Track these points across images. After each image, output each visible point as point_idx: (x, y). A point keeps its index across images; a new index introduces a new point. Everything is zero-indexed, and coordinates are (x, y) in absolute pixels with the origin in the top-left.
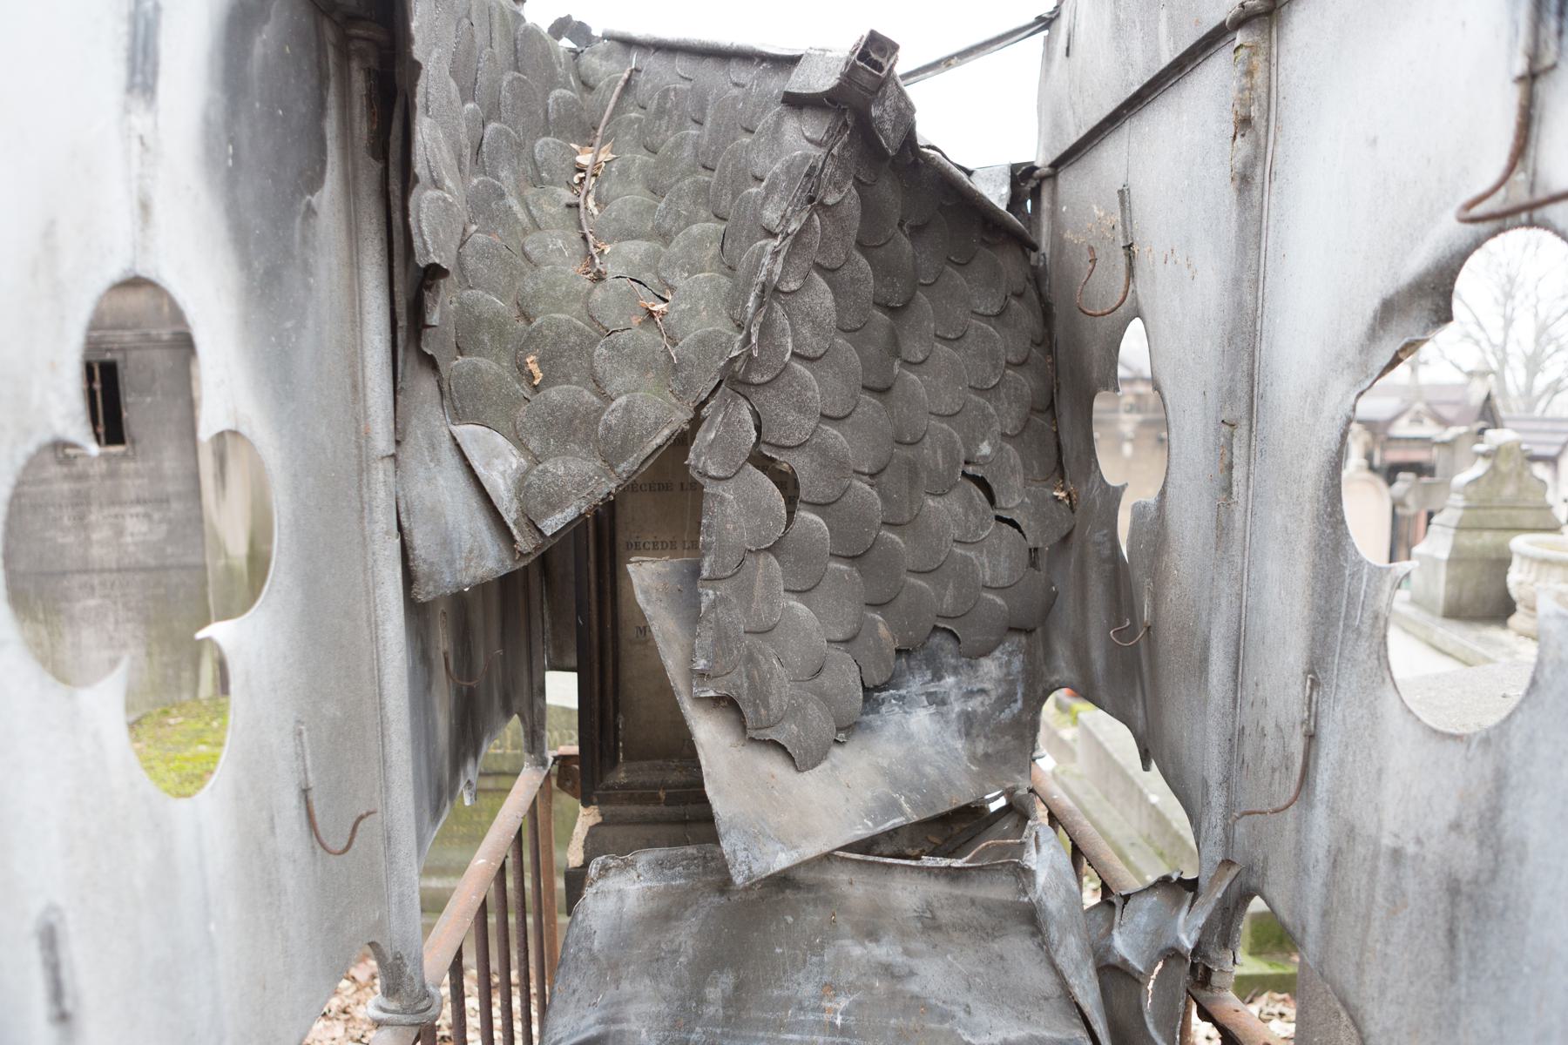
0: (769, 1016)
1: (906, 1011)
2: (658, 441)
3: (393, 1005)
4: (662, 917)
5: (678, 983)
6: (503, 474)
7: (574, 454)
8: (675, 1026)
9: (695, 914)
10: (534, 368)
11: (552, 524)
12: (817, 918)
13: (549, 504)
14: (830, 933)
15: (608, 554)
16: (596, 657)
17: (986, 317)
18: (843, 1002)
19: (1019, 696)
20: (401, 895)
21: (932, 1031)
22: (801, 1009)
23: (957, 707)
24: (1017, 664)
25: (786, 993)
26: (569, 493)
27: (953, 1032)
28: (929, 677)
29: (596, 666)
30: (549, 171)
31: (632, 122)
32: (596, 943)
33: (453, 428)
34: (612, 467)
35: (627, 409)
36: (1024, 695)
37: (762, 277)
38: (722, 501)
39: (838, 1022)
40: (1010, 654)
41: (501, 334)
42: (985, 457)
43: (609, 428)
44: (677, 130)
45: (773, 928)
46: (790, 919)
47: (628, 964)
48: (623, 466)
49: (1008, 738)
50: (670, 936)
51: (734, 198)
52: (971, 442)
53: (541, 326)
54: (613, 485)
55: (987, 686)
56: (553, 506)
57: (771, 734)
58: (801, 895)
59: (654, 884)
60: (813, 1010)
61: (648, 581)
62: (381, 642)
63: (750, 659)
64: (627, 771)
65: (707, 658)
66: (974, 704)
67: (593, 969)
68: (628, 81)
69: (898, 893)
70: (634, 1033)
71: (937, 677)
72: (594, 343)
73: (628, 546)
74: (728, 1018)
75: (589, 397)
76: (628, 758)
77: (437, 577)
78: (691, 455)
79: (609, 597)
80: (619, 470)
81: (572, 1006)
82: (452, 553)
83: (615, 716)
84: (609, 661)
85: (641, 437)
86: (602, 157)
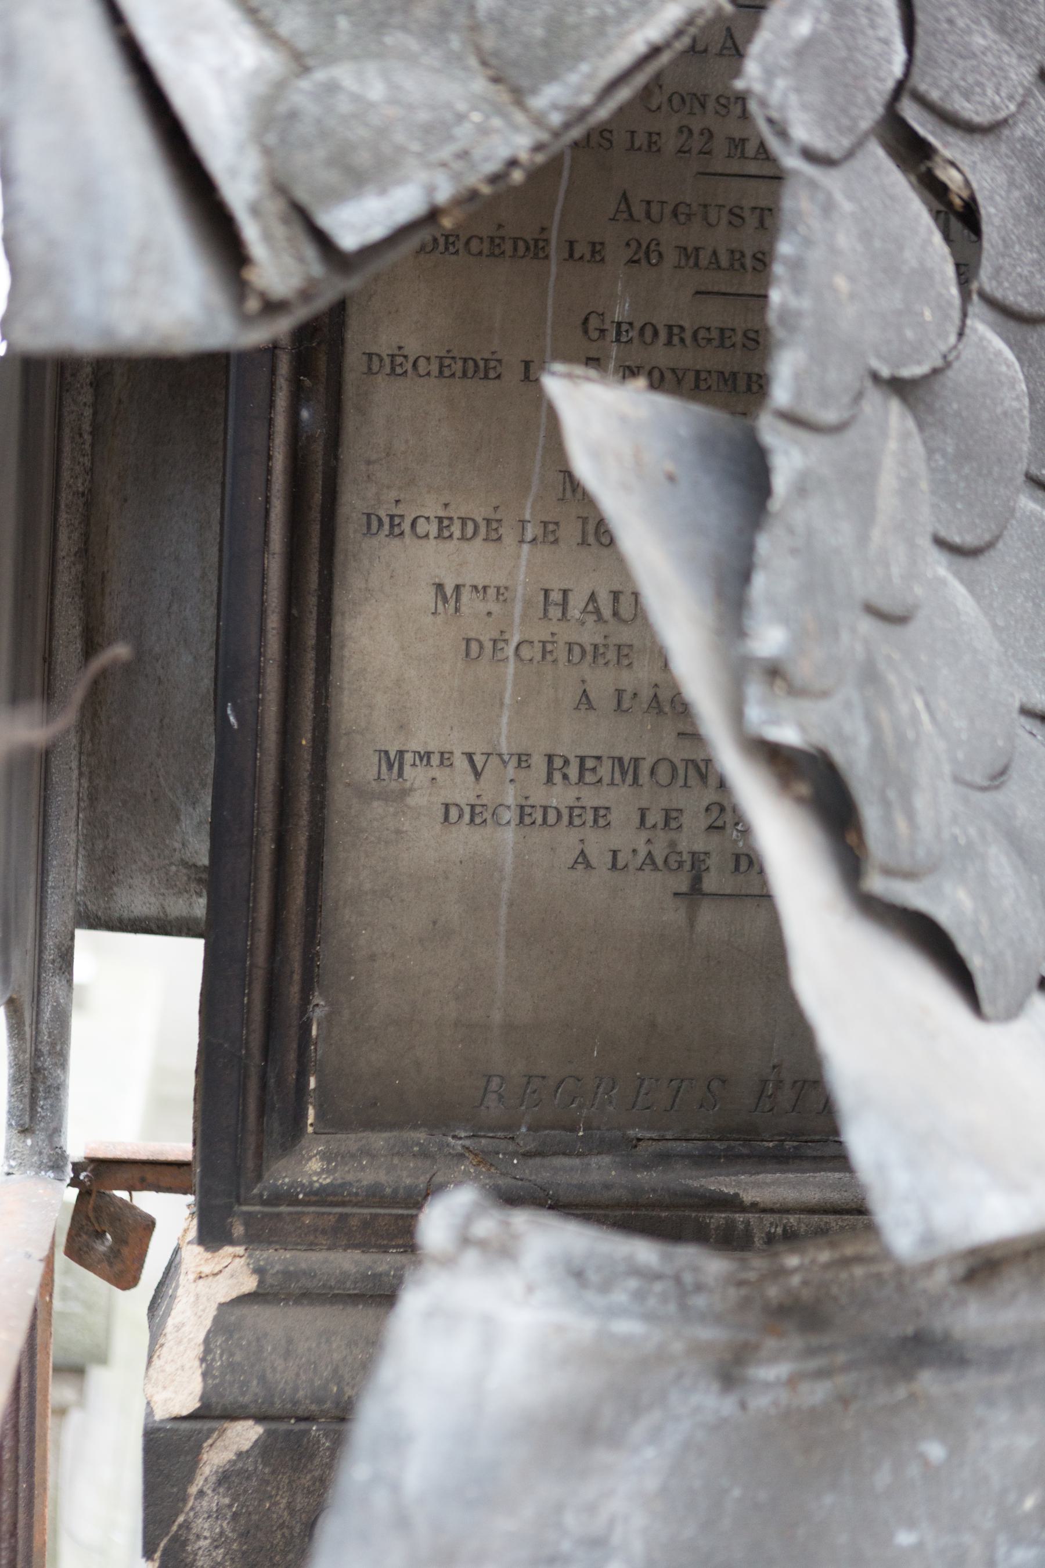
4: (580, 1430)
6: (220, 74)
7: (411, 59)
9: (655, 1435)
15: (315, 540)
26: (401, 150)
29: (268, 846)
34: (519, 96)
38: (828, 208)
45: (883, 1478)
46: (935, 1451)
56: (359, 177)
57: (913, 896)
58: (970, 1382)
63: (870, 676)
64: (326, 1157)
65: (785, 620)
73: (371, 523)
76: (330, 1122)
79: (310, 658)
85: (602, 21)
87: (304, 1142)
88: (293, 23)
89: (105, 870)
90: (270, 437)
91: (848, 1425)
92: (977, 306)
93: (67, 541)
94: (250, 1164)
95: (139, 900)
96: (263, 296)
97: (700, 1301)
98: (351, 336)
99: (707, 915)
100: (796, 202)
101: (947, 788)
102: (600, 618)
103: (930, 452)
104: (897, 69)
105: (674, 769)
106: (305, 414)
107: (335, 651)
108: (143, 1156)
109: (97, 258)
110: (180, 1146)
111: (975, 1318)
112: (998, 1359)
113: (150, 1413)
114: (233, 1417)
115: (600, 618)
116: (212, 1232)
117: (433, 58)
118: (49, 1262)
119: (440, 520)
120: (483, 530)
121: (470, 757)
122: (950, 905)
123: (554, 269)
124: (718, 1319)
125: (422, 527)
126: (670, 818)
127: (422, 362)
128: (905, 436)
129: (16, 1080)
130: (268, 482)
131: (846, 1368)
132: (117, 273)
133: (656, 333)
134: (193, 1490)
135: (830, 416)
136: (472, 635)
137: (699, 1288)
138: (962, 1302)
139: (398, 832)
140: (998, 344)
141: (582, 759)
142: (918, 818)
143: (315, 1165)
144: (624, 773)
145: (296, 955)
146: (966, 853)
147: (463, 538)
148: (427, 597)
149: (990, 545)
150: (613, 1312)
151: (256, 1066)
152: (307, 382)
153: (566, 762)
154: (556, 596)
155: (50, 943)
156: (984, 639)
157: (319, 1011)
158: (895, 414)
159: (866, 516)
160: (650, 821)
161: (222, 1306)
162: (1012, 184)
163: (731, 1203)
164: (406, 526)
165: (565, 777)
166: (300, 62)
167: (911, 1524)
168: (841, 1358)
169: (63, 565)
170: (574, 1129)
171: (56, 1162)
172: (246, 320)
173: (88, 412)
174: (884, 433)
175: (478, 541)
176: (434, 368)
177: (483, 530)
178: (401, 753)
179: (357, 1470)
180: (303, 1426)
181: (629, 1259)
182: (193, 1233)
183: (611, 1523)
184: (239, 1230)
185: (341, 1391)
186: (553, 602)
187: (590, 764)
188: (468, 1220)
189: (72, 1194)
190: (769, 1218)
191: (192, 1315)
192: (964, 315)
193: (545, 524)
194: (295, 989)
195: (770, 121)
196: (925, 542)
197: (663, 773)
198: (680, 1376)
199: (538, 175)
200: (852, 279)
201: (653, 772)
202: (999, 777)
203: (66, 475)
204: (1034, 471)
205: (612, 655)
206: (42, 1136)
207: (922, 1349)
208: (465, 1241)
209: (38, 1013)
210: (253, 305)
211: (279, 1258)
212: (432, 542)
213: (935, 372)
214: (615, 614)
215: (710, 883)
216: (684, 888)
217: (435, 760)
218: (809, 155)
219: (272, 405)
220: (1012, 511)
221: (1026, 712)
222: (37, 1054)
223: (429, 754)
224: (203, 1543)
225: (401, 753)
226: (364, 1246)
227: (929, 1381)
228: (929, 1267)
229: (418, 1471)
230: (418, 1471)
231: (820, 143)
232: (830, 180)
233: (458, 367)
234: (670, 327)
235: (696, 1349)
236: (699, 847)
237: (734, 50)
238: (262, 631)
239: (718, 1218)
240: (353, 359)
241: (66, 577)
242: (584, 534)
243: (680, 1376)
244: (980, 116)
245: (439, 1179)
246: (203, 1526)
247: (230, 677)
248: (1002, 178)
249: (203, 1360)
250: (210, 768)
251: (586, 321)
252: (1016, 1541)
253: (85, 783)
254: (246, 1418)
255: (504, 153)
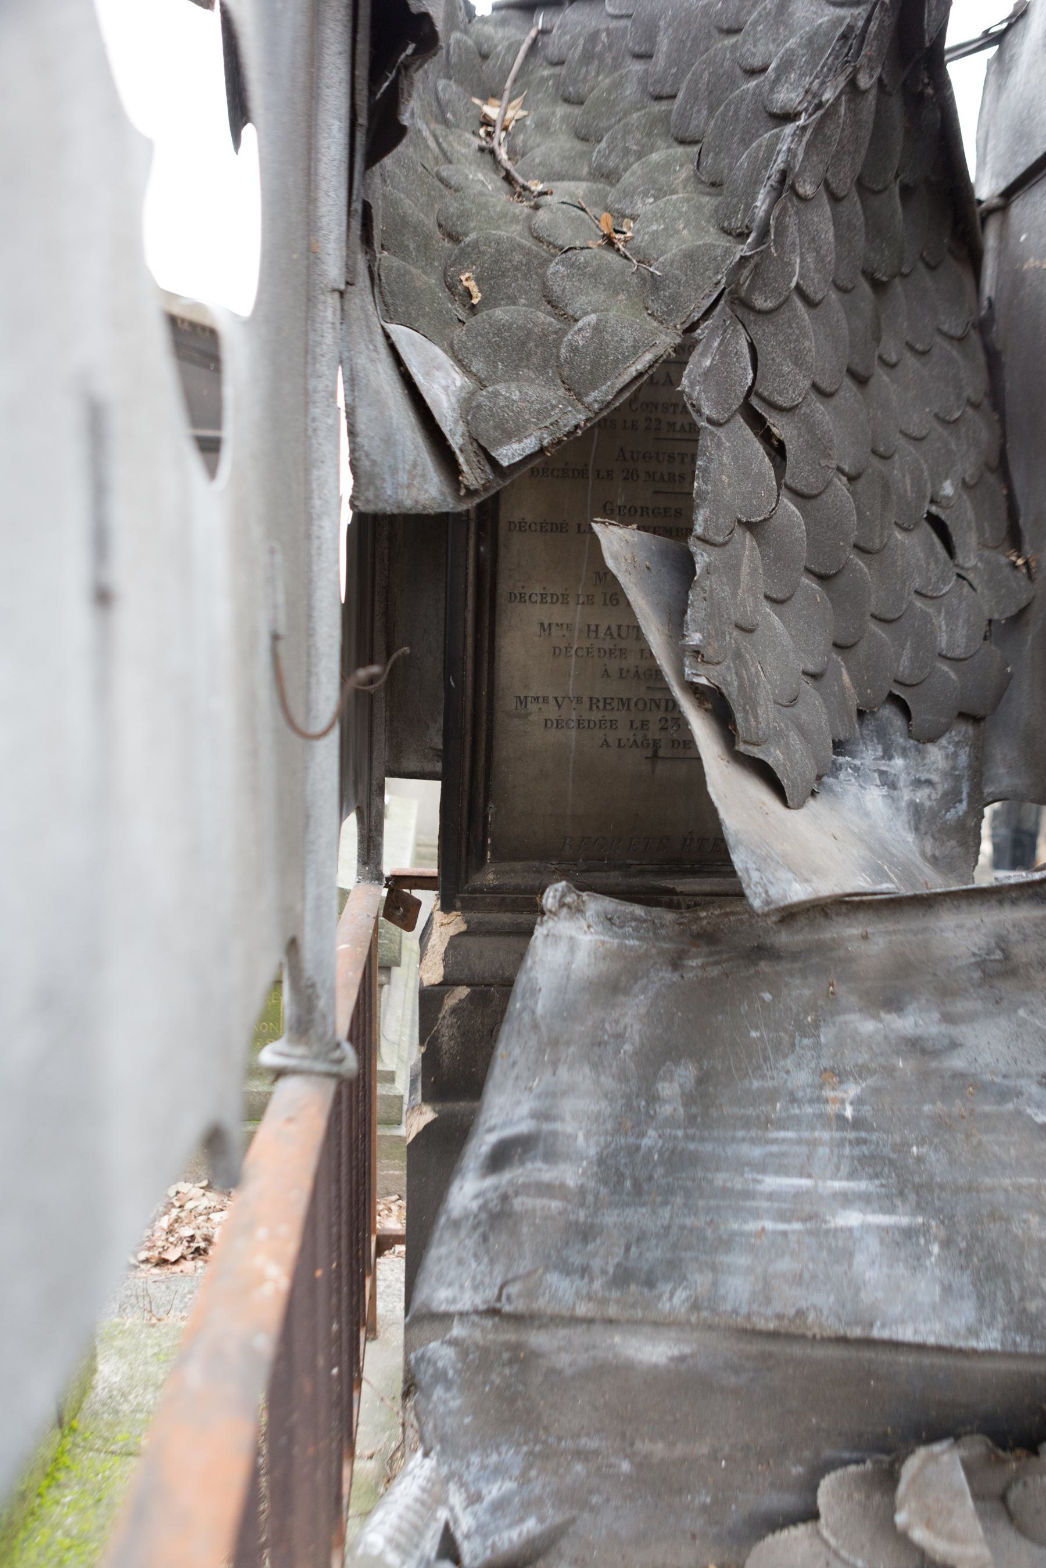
0: (750, 1111)
1: (945, 1094)
2: (640, 366)
3: (300, 1050)
4: (609, 988)
5: (622, 1077)
6: (446, 388)
7: (532, 381)
8: (619, 1129)
9: (644, 990)
10: (472, 285)
11: (508, 454)
12: (807, 992)
13: (504, 431)
14: (827, 1007)
16: (468, 727)
17: (951, 338)
18: (853, 1090)
19: (964, 795)
20: (319, 898)
21: (986, 1116)
22: (793, 1099)
23: (906, 795)
24: (963, 759)
25: (770, 1084)
26: (528, 421)
27: (1019, 1113)
28: (880, 753)
29: (468, 739)
30: (454, 114)
31: (544, 80)
32: (540, 1004)
33: (386, 325)
34: (579, 397)
35: (598, 329)
36: (969, 796)
37: (779, 163)
38: (719, 444)
39: (849, 1112)
40: (957, 744)
41: (426, 247)
42: (947, 498)
43: (574, 349)
44: (611, 73)
45: (744, 1008)
46: (767, 996)
47: (568, 1044)
48: (594, 394)
49: (953, 843)
50: (615, 1014)
51: (712, 110)
52: (937, 480)
53: (477, 241)
54: (581, 417)
55: (935, 777)
56: (509, 435)
58: (782, 966)
59: (606, 939)
60: (811, 1101)
61: (616, 547)
62: (316, 543)
63: (738, 655)
64: (495, 873)
65: (701, 630)
66: (921, 795)
67: (533, 1042)
68: (535, 41)
69: (949, 935)
70: (569, 1136)
71: (888, 755)
72: (545, 263)
74: (691, 1120)
75: (543, 317)
76: (498, 858)
77: (378, 482)
78: (685, 381)
80: (588, 399)
81: (510, 1083)
82: (395, 458)
83: (486, 805)
84: (483, 736)
85: (616, 361)
86: (510, 114)
87: (486, 867)
88: (478, 366)
89: (397, 751)
90: (467, 559)
91: (728, 985)
92: (784, 491)
93: (378, 609)
94: (463, 876)
95: (412, 766)
96: (467, 488)
97: (663, 932)
98: (503, 513)
99: (660, 766)
100: (706, 442)
101: (771, 705)
102: (612, 637)
103: (763, 557)
104: (750, 382)
105: (645, 703)
106: (482, 549)
107: (497, 653)
108: (416, 874)
109: (394, 471)
110: (432, 869)
111: (784, 938)
112: (795, 956)
113: (421, 983)
114: (458, 985)
115: (612, 637)
116: (447, 906)
117: (541, 380)
118: (377, 918)
119: (542, 595)
120: (560, 600)
121: (556, 699)
122: (774, 756)
123: (590, 483)
124: (671, 939)
125: (534, 598)
126: (644, 724)
127: (533, 526)
128: (752, 549)
129: (360, 842)
130: (466, 579)
131: (726, 961)
132: (403, 477)
133: (636, 511)
134: (441, 1016)
135: (720, 539)
136: (556, 645)
137: (662, 926)
138: (779, 932)
139: (525, 732)
140: (793, 508)
141: (605, 699)
142: (761, 717)
143: (491, 876)
144: (623, 705)
145: (482, 786)
146: (780, 734)
147: (552, 603)
148: (536, 629)
149: (789, 598)
150: (625, 936)
151: (463, 835)
152: (483, 535)
153: (598, 700)
154: (593, 628)
155: (374, 782)
156: (787, 641)
157: (492, 808)
158: (748, 540)
159: (736, 585)
160: (635, 726)
161: (451, 937)
162: (799, 435)
163: (672, 892)
164: (527, 597)
165: (598, 707)
166: (481, 384)
167: (757, 1028)
168: (725, 956)
169: (377, 618)
170: (603, 860)
171: (378, 876)
172: (459, 499)
173: (386, 552)
174: (743, 547)
175: (558, 604)
176: (538, 528)
177: (560, 600)
178: (526, 697)
179: (516, 1005)
180: (488, 988)
181: (632, 913)
182: (438, 906)
183: (625, 1028)
184: (458, 904)
185: (504, 973)
186: (592, 630)
187: (608, 701)
188: (563, 896)
189: (385, 892)
190: (688, 898)
191: (438, 942)
192: (779, 496)
193: (588, 596)
194: (481, 800)
195: (693, 406)
196: (762, 597)
197: (641, 705)
198: (655, 963)
199: (588, 432)
200: (729, 477)
201: (636, 704)
202: (793, 702)
203: (377, 579)
204: (808, 565)
205: (617, 653)
206: (372, 866)
207: (761, 952)
208: (562, 905)
209: (370, 813)
210: (463, 492)
211: (476, 916)
212: (538, 605)
213: (765, 520)
214: (619, 635)
215: (662, 753)
216: (650, 755)
217: (541, 700)
218: (710, 421)
219: (467, 545)
220: (799, 583)
221: (805, 673)
222: (370, 830)
223: (538, 698)
224: (445, 1039)
225: (526, 697)
226: (513, 911)
227: (764, 966)
228: (766, 915)
229: (542, 1005)
230: (542, 1005)
231: (714, 416)
232: (721, 433)
233: (549, 527)
234: (642, 508)
235: (661, 952)
236: (657, 737)
237: (673, 381)
238: (465, 645)
239: (666, 898)
240: (503, 525)
241: (378, 624)
242: (605, 600)
243: (655, 963)
244: (787, 404)
245: (544, 882)
246: (444, 1031)
247: (451, 664)
248: (795, 432)
249: (444, 960)
250: (442, 706)
251: (605, 506)
252: (804, 1035)
253: (388, 714)
254: (463, 985)
255: (574, 422)
